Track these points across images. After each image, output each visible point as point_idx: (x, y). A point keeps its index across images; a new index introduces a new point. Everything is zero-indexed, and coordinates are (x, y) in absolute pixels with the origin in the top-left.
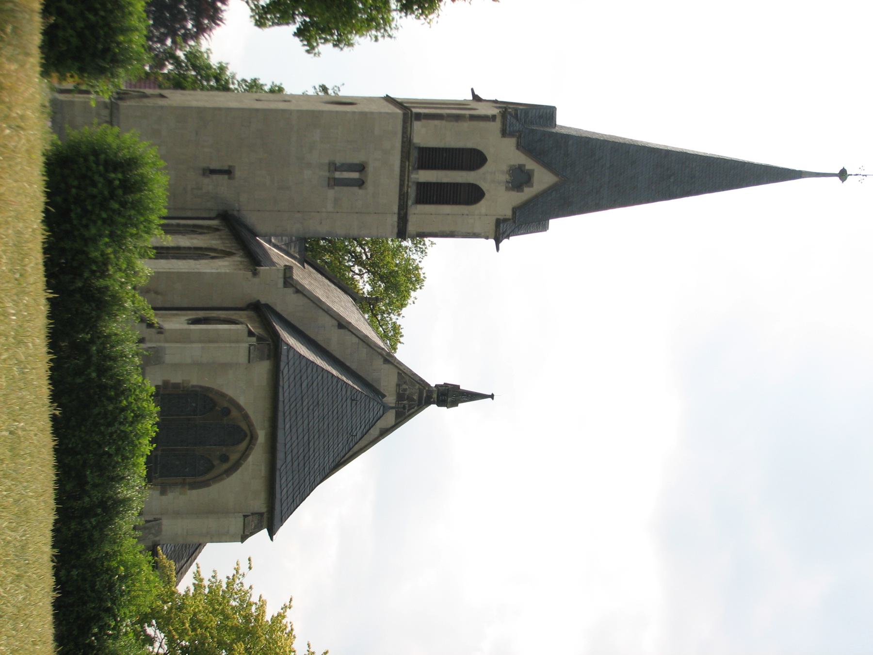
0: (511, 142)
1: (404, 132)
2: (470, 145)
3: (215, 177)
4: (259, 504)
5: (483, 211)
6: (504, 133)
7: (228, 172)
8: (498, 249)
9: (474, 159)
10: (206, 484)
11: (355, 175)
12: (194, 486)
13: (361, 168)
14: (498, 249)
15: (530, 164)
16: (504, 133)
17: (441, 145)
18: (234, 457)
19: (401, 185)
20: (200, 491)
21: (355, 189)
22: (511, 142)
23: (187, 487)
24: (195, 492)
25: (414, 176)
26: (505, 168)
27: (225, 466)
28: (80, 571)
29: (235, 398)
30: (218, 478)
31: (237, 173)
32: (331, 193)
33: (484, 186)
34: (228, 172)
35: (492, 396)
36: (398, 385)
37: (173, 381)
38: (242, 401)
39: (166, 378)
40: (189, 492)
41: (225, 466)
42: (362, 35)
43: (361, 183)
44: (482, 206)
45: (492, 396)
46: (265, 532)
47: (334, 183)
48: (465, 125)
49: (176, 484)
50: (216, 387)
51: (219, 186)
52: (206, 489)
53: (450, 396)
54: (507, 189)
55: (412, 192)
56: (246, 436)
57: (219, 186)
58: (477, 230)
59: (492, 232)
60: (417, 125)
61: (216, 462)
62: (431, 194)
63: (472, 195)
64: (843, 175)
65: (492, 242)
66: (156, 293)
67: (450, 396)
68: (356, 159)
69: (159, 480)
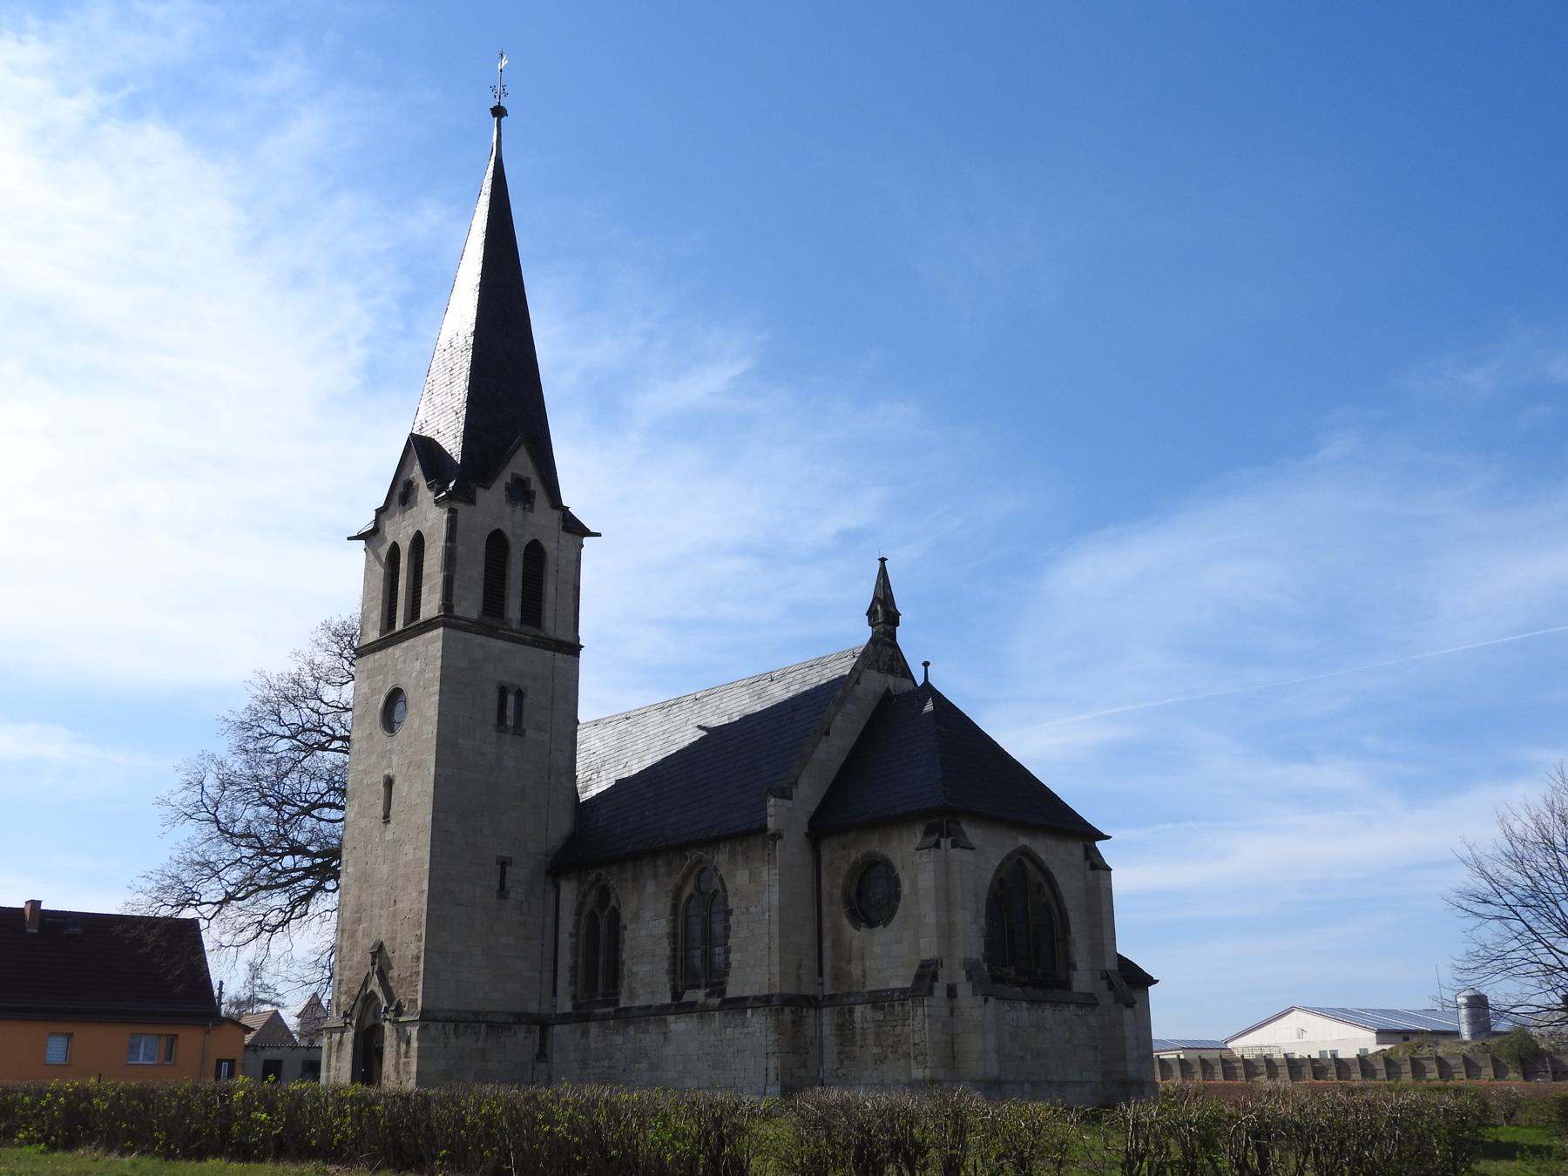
0: (482, 495)
1: (465, 629)
2: (482, 548)
3: (508, 884)
4: (1077, 849)
5: (554, 545)
6: (471, 501)
7: (504, 864)
8: (599, 535)
9: (497, 543)
10: (1063, 913)
11: (511, 699)
12: (1066, 929)
13: (503, 692)
14: (599, 535)
15: (505, 477)
16: (471, 501)
17: (481, 583)
18: (1040, 878)
19: (524, 642)
21: (526, 701)
22: (482, 495)
25: (514, 625)
26: (508, 509)
28: (1451, 1083)
31: (506, 854)
32: (531, 733)
33: (528, 539)
34: (504, 864)
35: (883, 560)
36: (879, 670)
43: (520, 695)
44: (549, 545)
45: (883, 560)
46: (1099, 844)
47: (519, 730)
48: (461, 549)
51: (519, 873)
53: (884, 612)
54: (531, 511)
55: (532, 630)
57: (519, 873)
58: (574, 557)
59: (577, 538)
60: (457, 611)
62: (533, 609)
63: (535, 553)
64: (498, 112)
65: (586, 540)
66: (800, 967)
67: (884, 612)
68: (493, 696)
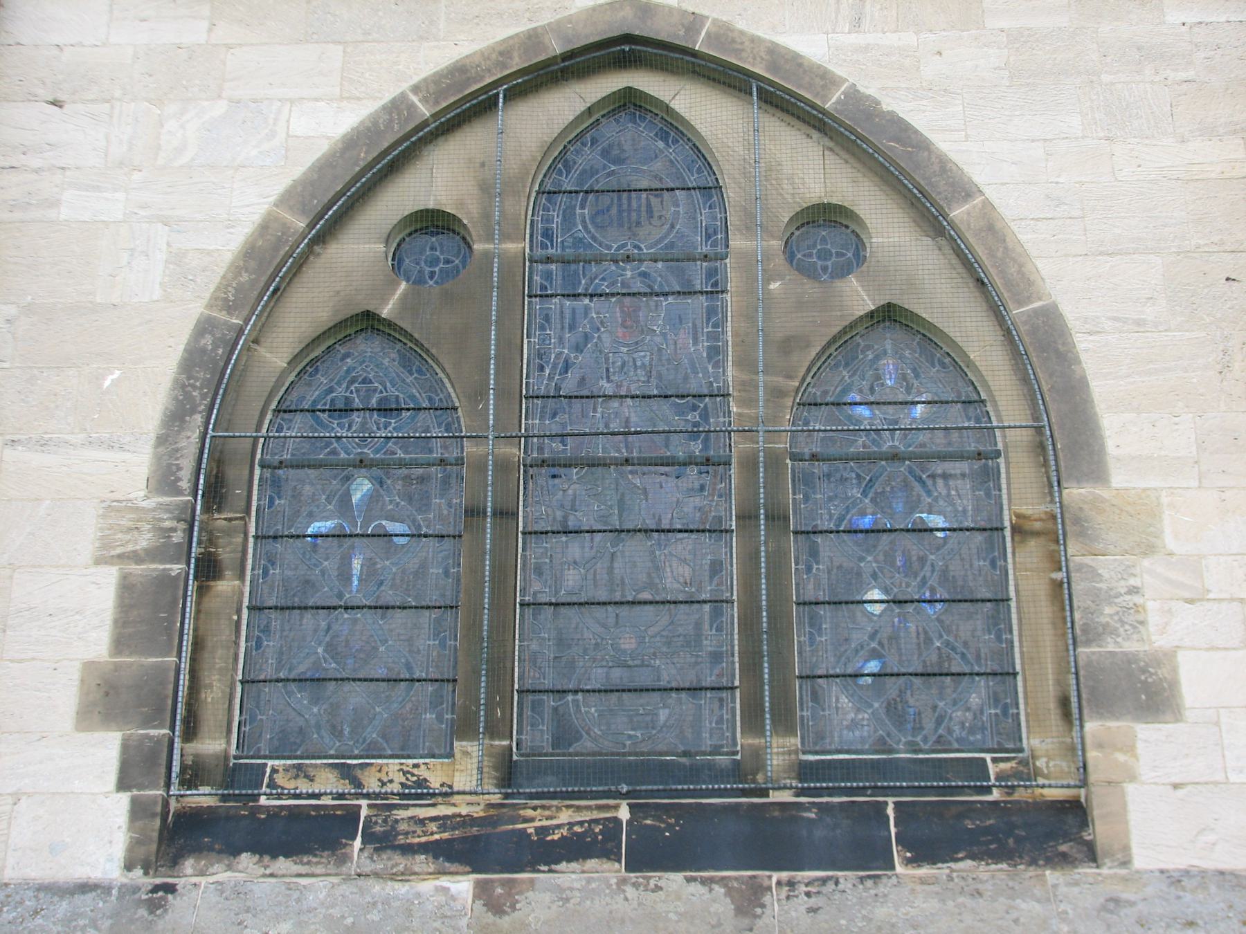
10: (1040, 351)
12: (1064, 437)
20: (1103, 388)
23: (1075, 493)
24: (1120, 431)
27: (888, 229)
29: (297, 171)
30: (984, 273)
37: (93, 639)
38: (323, 118)
39: (66, 697)
40: (1119, 478)
41: (888, 229)
42: (1053, 868)
49: (876, 174)
50: (193, 306)
52: (1083, 344)
56: (629, 102)
61: (858, 297)
69: (1041, 742)
